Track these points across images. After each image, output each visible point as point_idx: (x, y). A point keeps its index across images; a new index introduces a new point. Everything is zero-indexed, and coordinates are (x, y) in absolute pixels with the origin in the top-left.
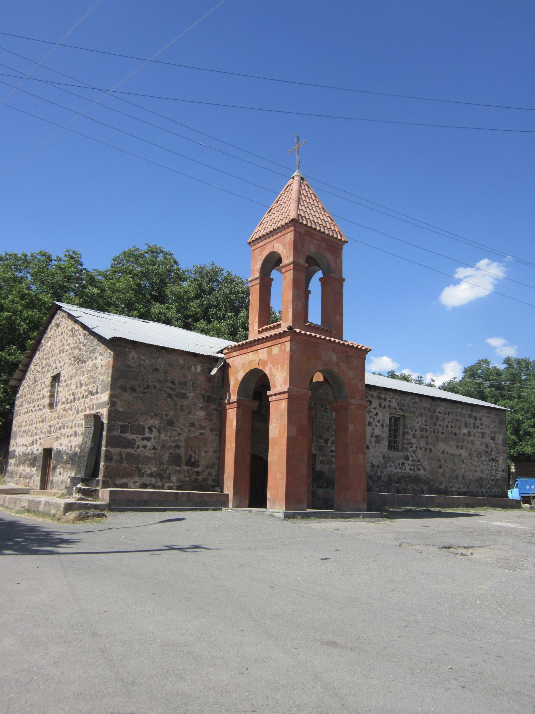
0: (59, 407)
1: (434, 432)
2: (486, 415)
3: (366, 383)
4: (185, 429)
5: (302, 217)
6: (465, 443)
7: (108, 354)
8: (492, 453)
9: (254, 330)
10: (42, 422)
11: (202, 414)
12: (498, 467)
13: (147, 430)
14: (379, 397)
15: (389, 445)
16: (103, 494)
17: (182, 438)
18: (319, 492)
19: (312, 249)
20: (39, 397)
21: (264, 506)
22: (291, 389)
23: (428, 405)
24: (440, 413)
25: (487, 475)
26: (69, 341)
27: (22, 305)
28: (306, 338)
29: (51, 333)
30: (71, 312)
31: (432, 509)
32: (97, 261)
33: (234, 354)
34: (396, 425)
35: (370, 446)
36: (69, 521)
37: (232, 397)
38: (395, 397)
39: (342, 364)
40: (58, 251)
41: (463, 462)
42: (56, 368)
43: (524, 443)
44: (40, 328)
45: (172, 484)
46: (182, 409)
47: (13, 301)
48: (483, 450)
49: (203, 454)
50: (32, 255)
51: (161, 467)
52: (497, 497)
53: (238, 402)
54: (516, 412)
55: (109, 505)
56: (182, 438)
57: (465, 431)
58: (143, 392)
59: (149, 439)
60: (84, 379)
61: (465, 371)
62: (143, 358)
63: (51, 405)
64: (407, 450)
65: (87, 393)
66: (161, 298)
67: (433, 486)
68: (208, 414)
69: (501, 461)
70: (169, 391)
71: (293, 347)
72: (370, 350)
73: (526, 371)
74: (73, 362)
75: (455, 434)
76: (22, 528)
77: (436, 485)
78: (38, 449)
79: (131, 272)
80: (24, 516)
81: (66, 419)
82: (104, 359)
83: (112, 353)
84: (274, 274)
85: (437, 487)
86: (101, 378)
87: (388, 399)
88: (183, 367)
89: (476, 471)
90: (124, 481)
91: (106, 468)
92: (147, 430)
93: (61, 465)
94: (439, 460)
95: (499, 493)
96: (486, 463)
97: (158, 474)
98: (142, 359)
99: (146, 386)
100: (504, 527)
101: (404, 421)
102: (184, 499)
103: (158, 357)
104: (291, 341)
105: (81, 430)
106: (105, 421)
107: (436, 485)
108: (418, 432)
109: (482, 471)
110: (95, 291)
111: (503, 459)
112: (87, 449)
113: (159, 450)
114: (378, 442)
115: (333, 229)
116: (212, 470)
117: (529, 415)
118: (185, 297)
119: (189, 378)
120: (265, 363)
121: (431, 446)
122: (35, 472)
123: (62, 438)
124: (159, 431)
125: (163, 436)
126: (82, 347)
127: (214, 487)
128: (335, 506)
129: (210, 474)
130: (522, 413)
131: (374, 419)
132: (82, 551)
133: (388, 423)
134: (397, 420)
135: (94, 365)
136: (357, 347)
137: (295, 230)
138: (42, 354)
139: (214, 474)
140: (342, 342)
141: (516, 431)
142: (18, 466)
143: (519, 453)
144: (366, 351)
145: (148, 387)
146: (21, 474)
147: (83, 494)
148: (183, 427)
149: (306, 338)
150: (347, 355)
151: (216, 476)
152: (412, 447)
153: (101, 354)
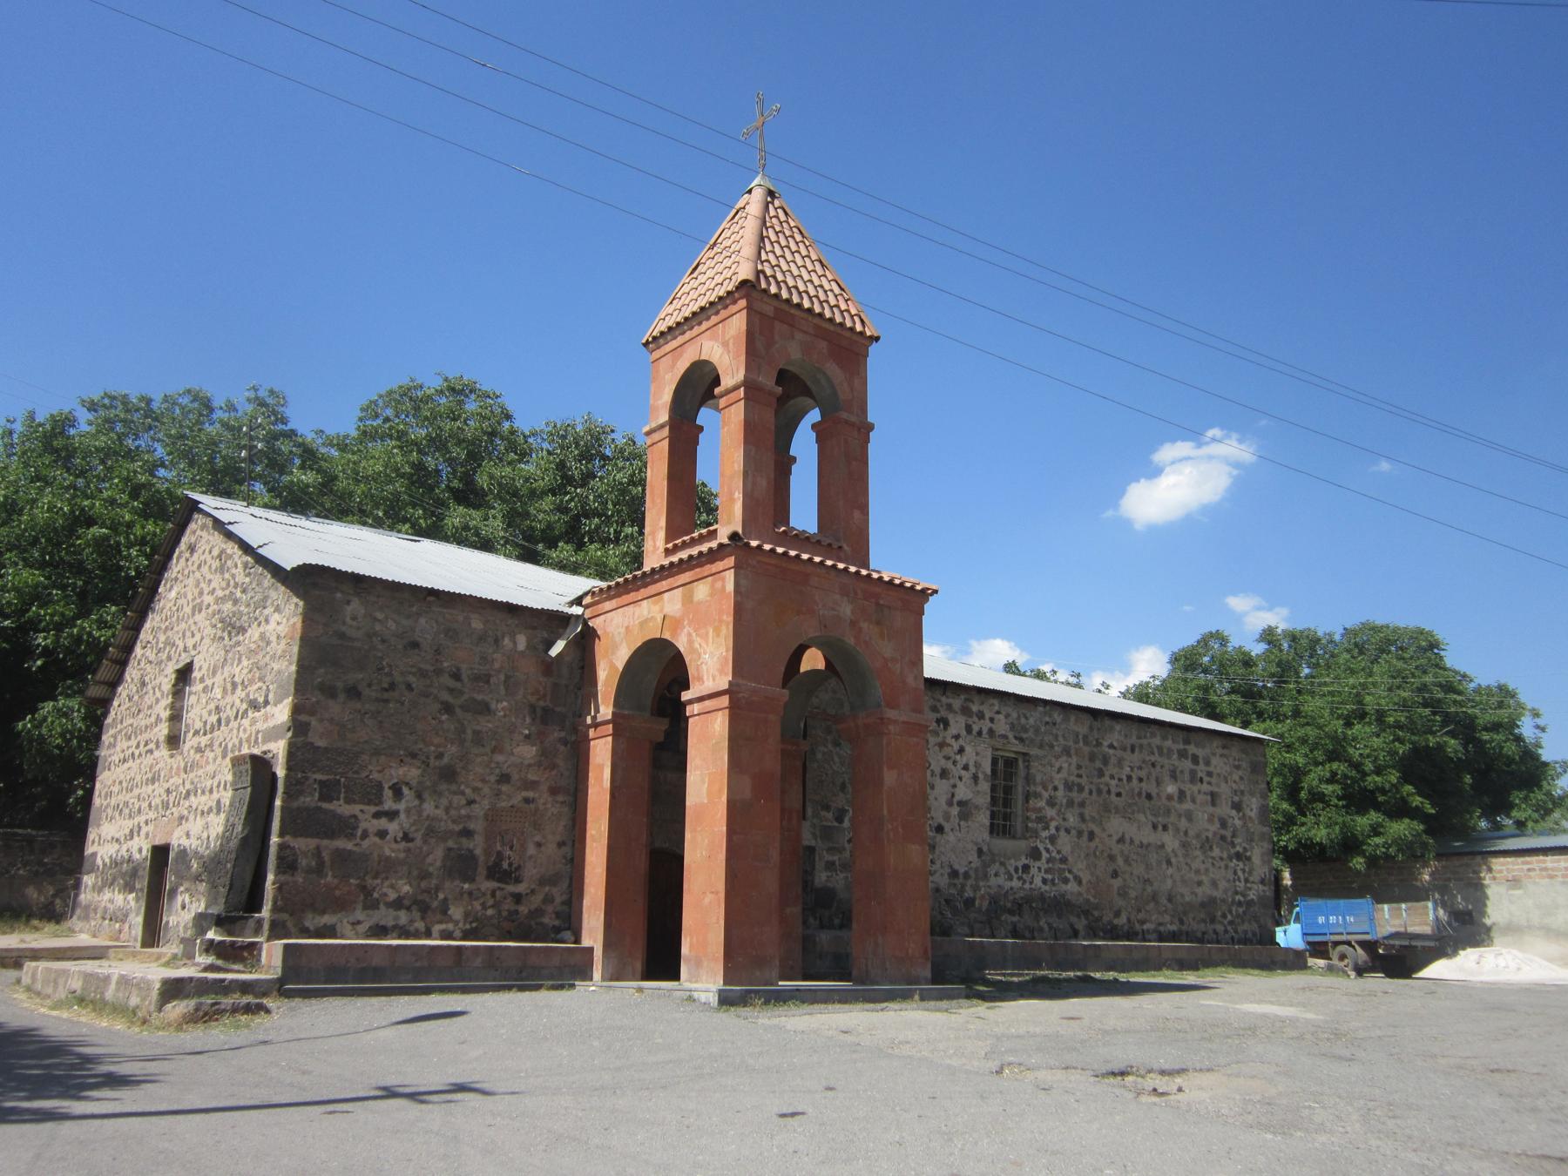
0: (190, 743)
1: (1099, 792)
2: (1219, 751)
3: (927, 674)
4: (486, 790)
5: (766, 278)
6: (1173, 819)
7: (293, 607)
8: (1237, 841)
9: (655, 548)
10: (153, 781)
11: (528, 752)
12: (1250, 873)
13: (388, 793)
14: (966, 711)
15: (992, 825)
16: (270, 956)
17: (478, 810)
18: (812, 937)
19: (792, 352)
20: (148, 721)
21: (676, 976)
22: (738, 685)
23: (1083, 729)
24: (1111, 746)
25: (1225, 891)
26: (214, 584)
27: (134, 511)
28: (773, 561)
29: (179, 567)
30: (216, 514)
31: (1098, 975)
32: (325, 413)
33: (608, 605)
34: (1009, 776)
35: (947, 827)
36: (169, 1025)
37: (602, 709)
38: (1005, 710)
39: (864, 625)
40: (231, 391)
41: (1169, 863)
42: (185, 650)
43: (1310, 819)
44: (161, 556)
45: (450, 926)
46: (478, 739)
47: (112, 502)
48: (1215, 834)
49: (531, 850)
50: (166, 399)
51: (423, 884)
52: (1251, 943)
53: (616, 720)
54: (1289, 748)
55: (281, 981)
56: (478, 810)
57: (1171, 789)
58: (377, 700)
59: (392, 815)
60: (240, 671)
61: (1175, 659)
62: (380, 616)
63: (174, 741)
64: (1036, 835)
65: (244, 706)
66: (469, 495)
67: (1098, 919)
68: (544, 753)
69: (1256, 859)
70: (445, 696)
71: (743, 582)
72: (936, 592)
73: (1311, 656)
74: (219, 633)
75: (1149, 797)
76: (31, 1047)
77: (1106, 919)
78: (140, 848)
79: (401, 435)
80: (65, 1015)
81: (200, 772)
82: (281, 622)
83: (301, 603)
84: (705, 416)
85: (1110, 922)
86: (276, 666)
87: (987, 716)
88: (482, 638)
89: (1200, 883)
90: (327, 919)
91: (280, 888)
92: (388, 793)
93: (186, 885)
94: (1112, 858)
95: (1254, 934)
96: (1222, 864)
97: (415, 902)
98: (375, 619)
99: (386, 686)
100: (1264, 1016)
101: (1028, 767)
102: (478, 962)
103: (419, 615)
104: (737, 567)
105: (227, 796)
106: (280, 772)
107: (1106, 919)
108: (1060, 793)
109: (1214, 884)
110: (309, 478)
111: (1263, 855)
112: (234, 844)
113: (418, 842)
114: (964, 816)
115: (843, 307)
116: (555, 890)
117: (1319, 755)
118: (524, 491)
119: (497, 666)
120: (676, 624)
121: (1092, 826)
122: (133, 903)
123: (191, 817)
124: (419, 796)
125: (429, 807)
126: (239, 594)
127: (558, 930)
128: (855, 973)
129: (548, 899)
130: (1305, 750)
131: (955, 763)
132: (221, 1105)
133: (989, 771)
134: (1010, 763)
135: (262, 636)
136: (902, 584)
137: (749, 308)
138: (158, 618)
139: (558, 900)
140: (864, 572)
141: (1292, 793)
142: (100, 890)
143: (1299, 842)
144: (925, 594)
145: (392, 686)
146: (105, 910)
147: (219, 956)
148: (479, 785)
149: (773, 561)
150: (877, 604)
151: (563, 903)
152: (1047, 828)
153: (277, 610)
